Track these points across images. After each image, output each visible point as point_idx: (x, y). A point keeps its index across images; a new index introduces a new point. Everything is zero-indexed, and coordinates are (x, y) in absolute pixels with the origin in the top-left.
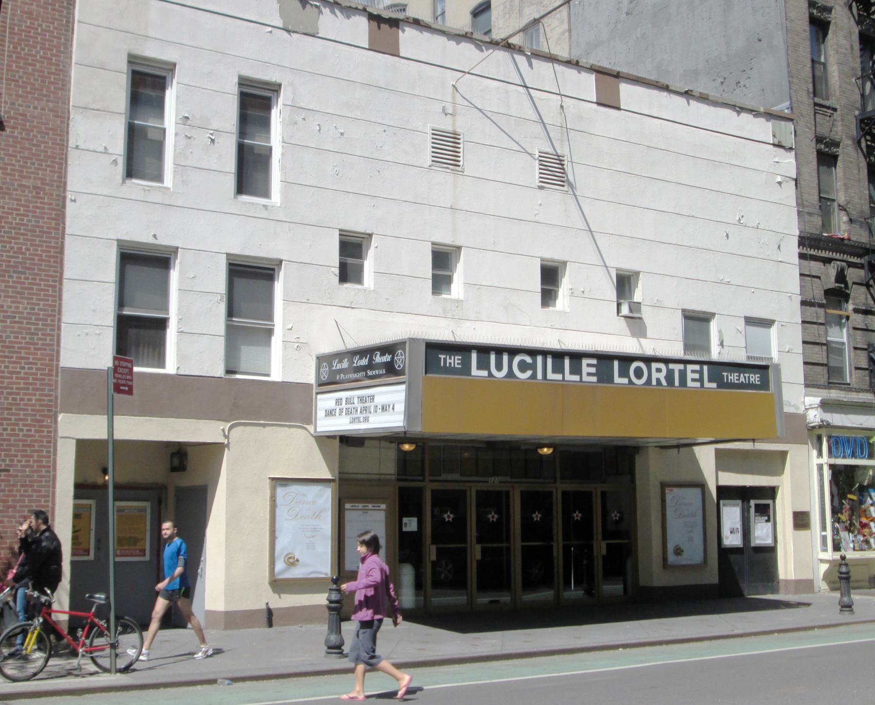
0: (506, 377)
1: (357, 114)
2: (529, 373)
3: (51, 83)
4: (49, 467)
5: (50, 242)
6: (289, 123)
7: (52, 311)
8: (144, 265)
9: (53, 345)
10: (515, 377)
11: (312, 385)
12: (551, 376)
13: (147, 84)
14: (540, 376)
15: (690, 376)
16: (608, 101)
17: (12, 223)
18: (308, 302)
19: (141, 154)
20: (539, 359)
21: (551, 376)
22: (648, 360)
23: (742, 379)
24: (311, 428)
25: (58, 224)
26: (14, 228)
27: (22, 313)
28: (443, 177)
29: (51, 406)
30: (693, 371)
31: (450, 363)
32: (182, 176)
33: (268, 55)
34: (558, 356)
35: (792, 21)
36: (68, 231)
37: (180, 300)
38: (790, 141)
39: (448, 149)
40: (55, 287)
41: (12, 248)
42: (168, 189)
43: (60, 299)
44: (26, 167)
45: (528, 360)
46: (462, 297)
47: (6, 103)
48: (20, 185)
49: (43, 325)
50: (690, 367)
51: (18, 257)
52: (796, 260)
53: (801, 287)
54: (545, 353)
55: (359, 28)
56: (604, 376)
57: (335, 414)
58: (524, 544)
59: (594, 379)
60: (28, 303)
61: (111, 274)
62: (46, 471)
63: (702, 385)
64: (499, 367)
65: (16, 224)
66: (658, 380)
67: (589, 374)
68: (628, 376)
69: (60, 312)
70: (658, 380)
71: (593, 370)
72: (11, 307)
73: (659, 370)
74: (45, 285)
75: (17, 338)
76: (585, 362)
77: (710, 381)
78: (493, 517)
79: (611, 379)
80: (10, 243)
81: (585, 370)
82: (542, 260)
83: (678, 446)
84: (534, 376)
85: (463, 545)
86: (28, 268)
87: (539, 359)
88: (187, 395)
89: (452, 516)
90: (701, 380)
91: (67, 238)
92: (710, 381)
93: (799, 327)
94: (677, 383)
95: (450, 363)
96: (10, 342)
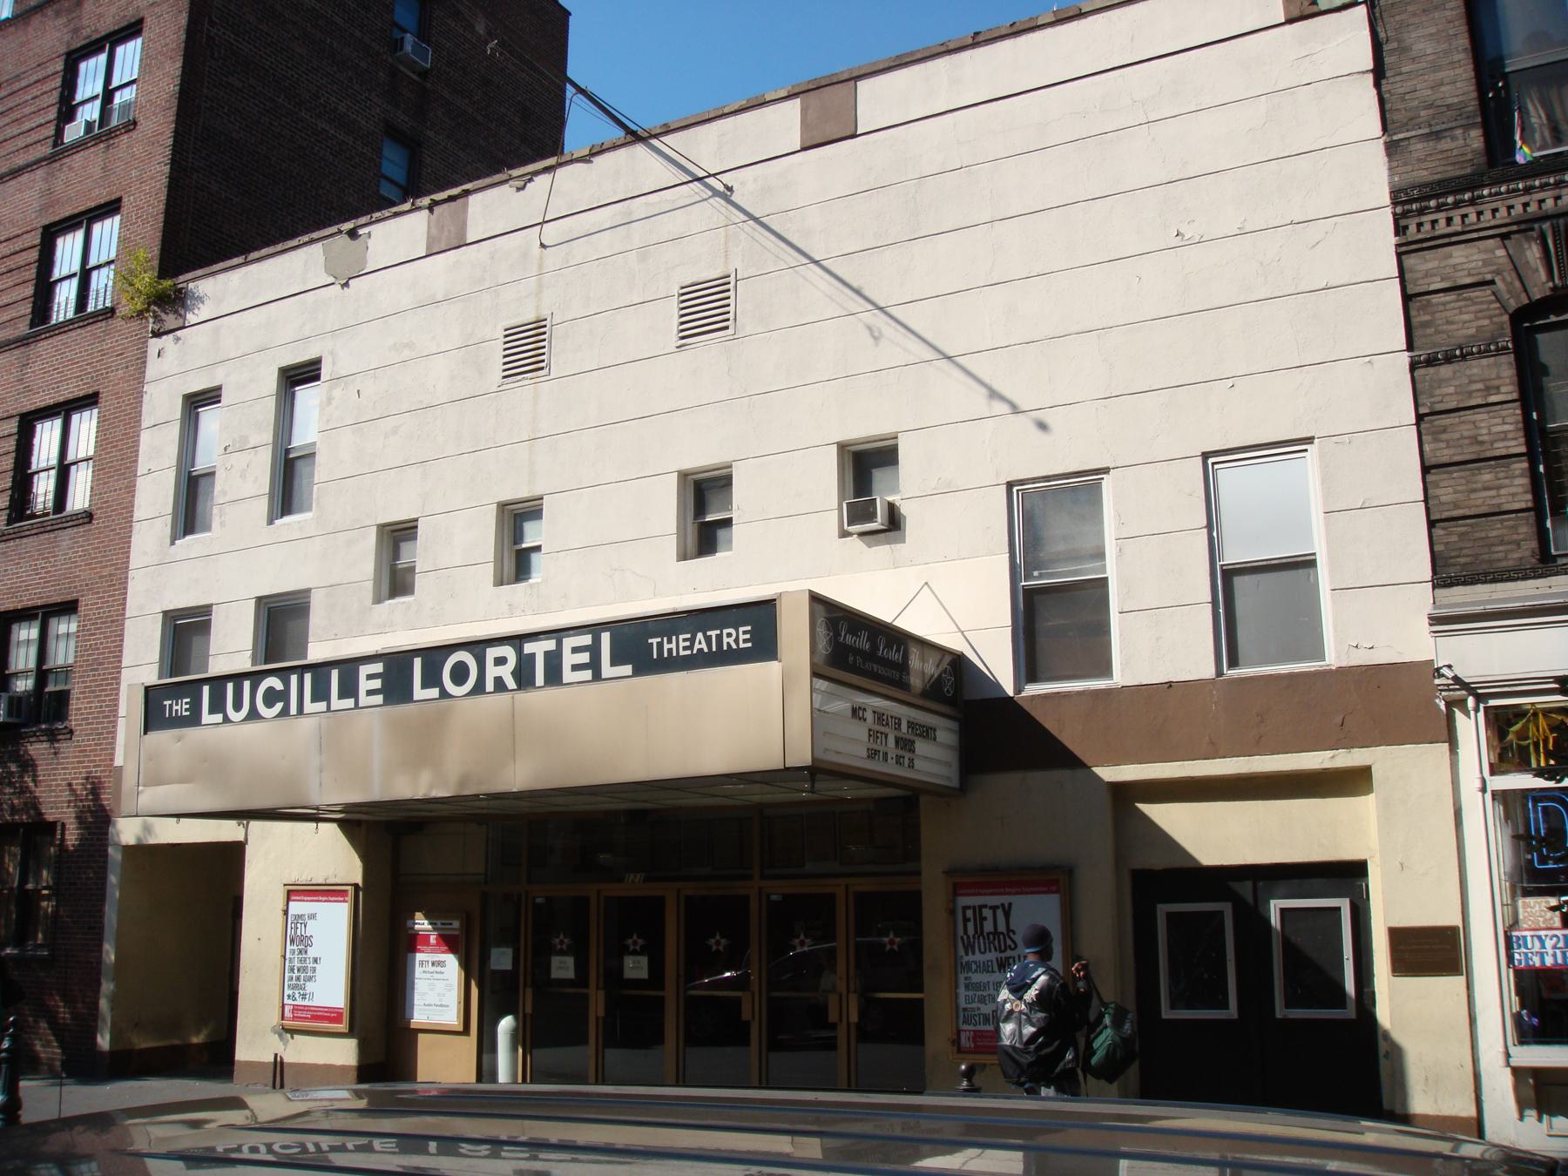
1: (406, 354)
2: (279, 706)
10: (451, 696)
15: (569, 659)
19: (190, 512)
20: (294, 678)
21: (309, 706)
22: (477, 647)
23: (700, 644)
31: (670, 650)
50: (569, 642)
58: (660, 993)
63: (597, 676)
64: (238, 706)
66: (500, 685)
68: (438, 682)
73: (500, 661)
76: (365, 670)
77: (614, 663)
78: (718, 943)
79: (405, 695)
81: (364, 685)
85: (775, 994)
87: (294, 678)
89: (723, 941)
95: (670, 650)
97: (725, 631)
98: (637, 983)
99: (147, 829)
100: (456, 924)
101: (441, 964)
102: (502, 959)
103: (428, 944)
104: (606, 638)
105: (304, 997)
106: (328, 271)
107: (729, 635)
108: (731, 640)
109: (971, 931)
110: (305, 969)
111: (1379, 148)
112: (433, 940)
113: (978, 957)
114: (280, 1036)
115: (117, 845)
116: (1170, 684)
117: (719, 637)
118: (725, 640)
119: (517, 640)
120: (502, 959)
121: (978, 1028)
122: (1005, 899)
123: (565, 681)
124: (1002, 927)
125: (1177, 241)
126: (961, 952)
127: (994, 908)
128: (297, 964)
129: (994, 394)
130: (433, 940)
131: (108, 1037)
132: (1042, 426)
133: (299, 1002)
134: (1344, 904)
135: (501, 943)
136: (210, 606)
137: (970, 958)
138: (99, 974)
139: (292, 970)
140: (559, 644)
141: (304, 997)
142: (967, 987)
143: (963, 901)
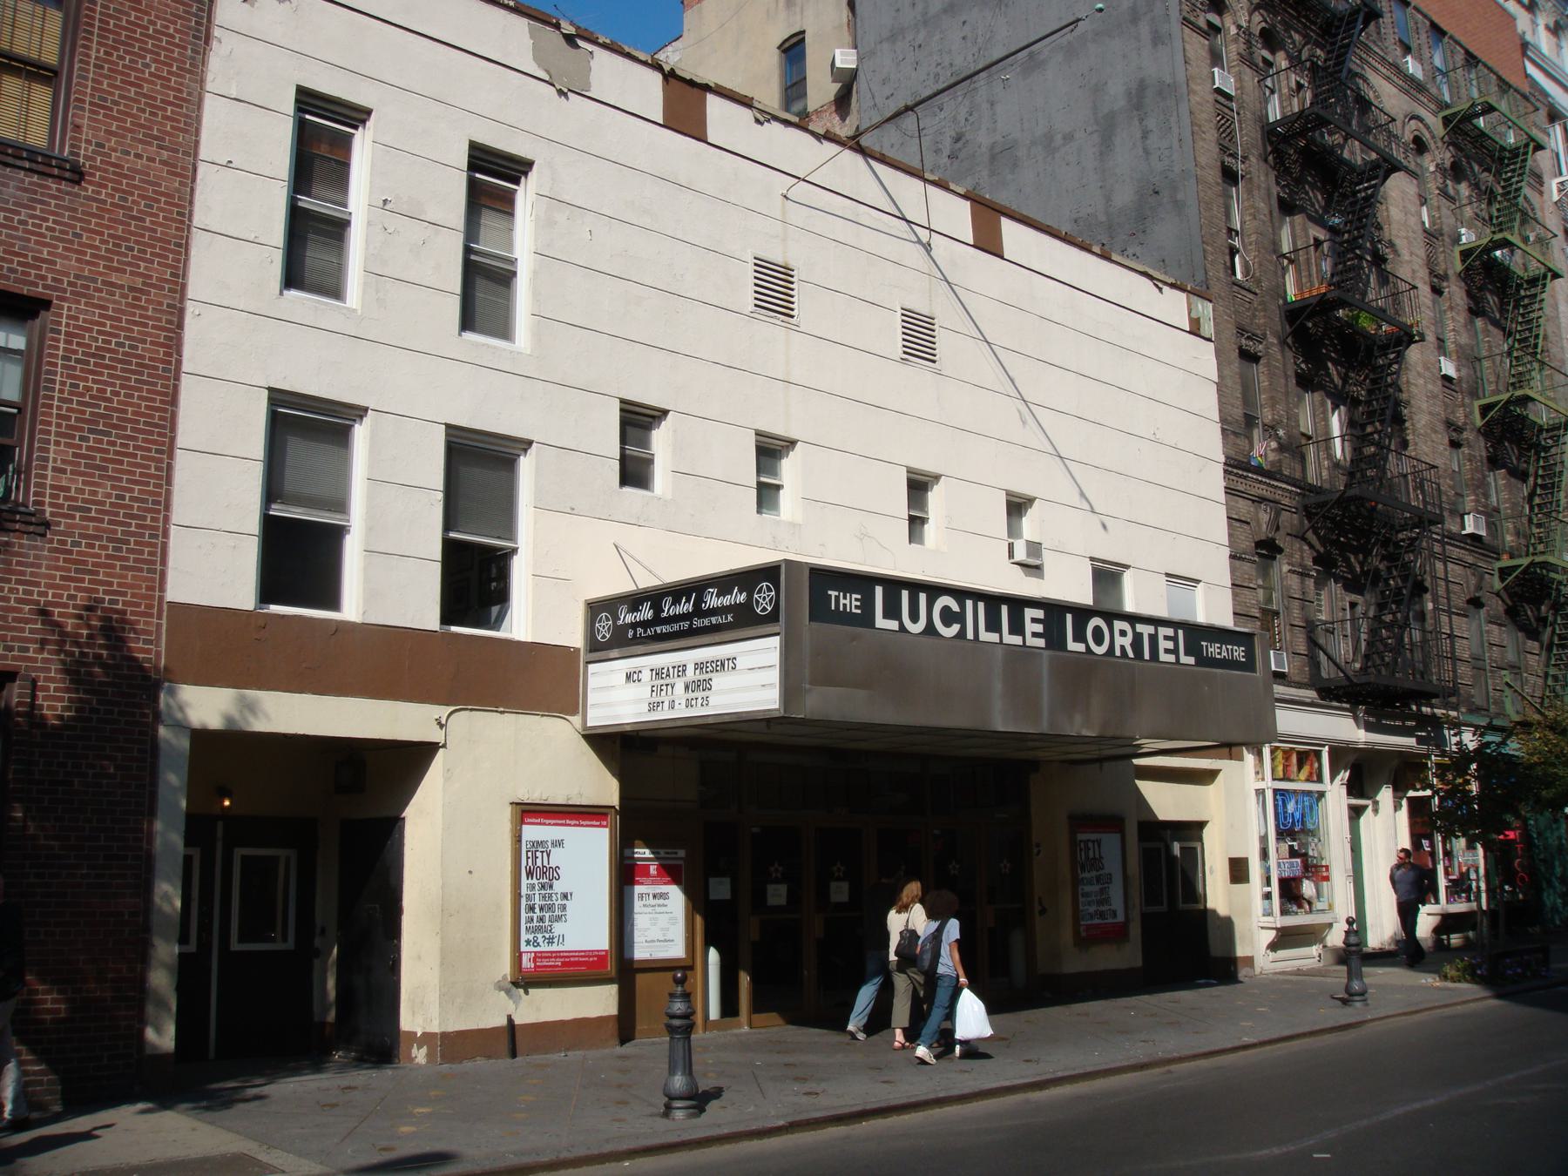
1: (645, 221)
2: (956, 628)
3: (165, 117)
4: (157, 528)
5: (155, 384)
6: (545, 224)
7: (154, 502)
8: (306, 429)
9: (154, 563)
11: (577, 650)
12: (985, 636)
13: (322, 135)
14: (970, 635)
15: (1164, 645)
16: (988, 242)
17: (89, 346)
18: (572, 512)
19: (311, 248)
20: (969, 603)
24: (576, 720)
25: (170, 355)
26: (94, 355)
27: (102, 503)
28: (769, 329)
29: (164, 427)
30: (1166, 638)
32: (377, 292)
33: (518, 115)
35: (1202, 168)
36: (186, 367)
37: (370, 497)
38: (1208, 328)
39: (775, 289)
40: (160, 461)
41: (88, 389)
42: (354, 310)
43: (169, 482)
44: (118, 254)
46: (799, 519)
47: (88, 142)
48: (104, 282)
49: (138, 526)
50: (1164, 631)
51: (99, 406)
52: (1222, 497)
53: (1230, 535)
54: (977, 596)
55: (647, 91)
56: (1054, 636)
57: (622, 694)
59: (1041, 642)
60: (113, 487)
61: (255, 443)
62: (177, 229)
63: (1178, 658)
64: (914, 617)
65: (97, 348)
66: (1122, 647)
67: (1035, 635)
68: (1084, 640)
69: (167, 507)
70: (1122, 647)
71: (1039, 628)
72: (82, 491)
73: (1123, 633)
74: (143, 457)
75: (92, 546)
77: (1186, 654)
80: (86, 380)
81: (1030, 627)
83: (1101, 760)
84: (962, 634)
86: (115, 427)
87: (969, 603)
88: (385, 661)
90: (1175, 651)
91: (184, 379)
92: (1186, 654)
93: (1228, 594)
94: (1147, 656)
96: (79, 553)
98: (778, 909)
99: (251, 708)
100: (682, 853)
101: (664, 896)
102: (720, 889)
103: (648, 875)
105: (550, 941)
106: (538, 58)
110: (550, 908)
111: (1217, 428)
112: (653, 870)
114: (508, 992)
115: (181, 726)
120: (720, 889)
128: (537, 901)
129: (1082, 495)
130: (653, 870)
131: (171, 1030)
132: (1104, 527)
133: (544, 947)
135: (720, 873)
136: (366, 410)
138: (147, 929)
139: (532, 909)
141: (550, 941)
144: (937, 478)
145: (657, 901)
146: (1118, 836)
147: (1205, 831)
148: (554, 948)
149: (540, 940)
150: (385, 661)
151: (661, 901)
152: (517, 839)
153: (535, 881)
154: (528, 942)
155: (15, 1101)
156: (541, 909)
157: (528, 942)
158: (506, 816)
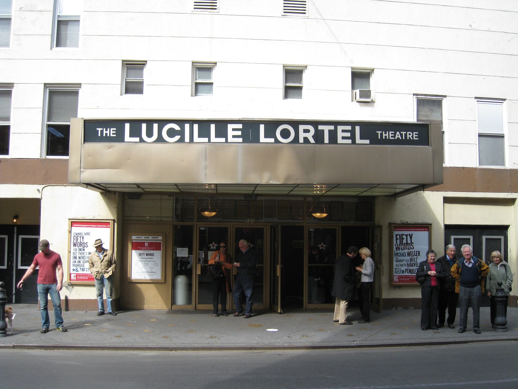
0: (157, 141)
2: (177, 138)
10: (164, 141)
14: (187, 139)
15: (340, 134)
20: (187, 126)
21: (196, 138)
22: (295, 124)
23: (398, 135)
31: (106, 134)
34: (204, 125)
45: (177, 127)
50: (340, 128)
54: (192, 122)
63: (354, 142)
64: (150, 134)
66: (306, 140)
68: (139, 135)
70: (306, 140)
73: (306, 131)
76: (230, 127)
77: (361, 138)
78: (322, 246)
79: (256, 139)
81: (230, 133)
82: (352, 68)
87: (187, 126)
88: (24, 171)
90: (353, 137)
94: (326, 140)
95: (106, 134)
97: (408, 133)
101: (152, 255)
104: (358, 128)
107: (410, 134)
108: (410, 136)
109: (398, 243)
113: (401, 251)
116: (463, 168)
117: (406, 135)
118: (408, 136)
119: (315, 124)
121: (400, 274)
122: (411, 233)
123: (125, 141)
124: (409, 242)
125: (469, 28)
126: (395, 249)
127: (407, 235)
128: (78, 255)
133: (80, 272)
134: (502, 238)
135: (183, 246)
136: (13, 84)
137: (398, 251)
139: (75, 258)
140: (336, 128)
142: (396, 261)
143: (395, 233)
144: (306, 67)
145: (148, 257)
146: (427, 232)
147: (509, 230)
148: (83, 272)
149: (79, 269)
150: (24, 171)
151: (150, 257)
152: (70, 232)
153: (77, 247)
154: (74, 270)
155: (445, 313)
156: (79, 258)
157: (74, 270)
158: (67, 224)
